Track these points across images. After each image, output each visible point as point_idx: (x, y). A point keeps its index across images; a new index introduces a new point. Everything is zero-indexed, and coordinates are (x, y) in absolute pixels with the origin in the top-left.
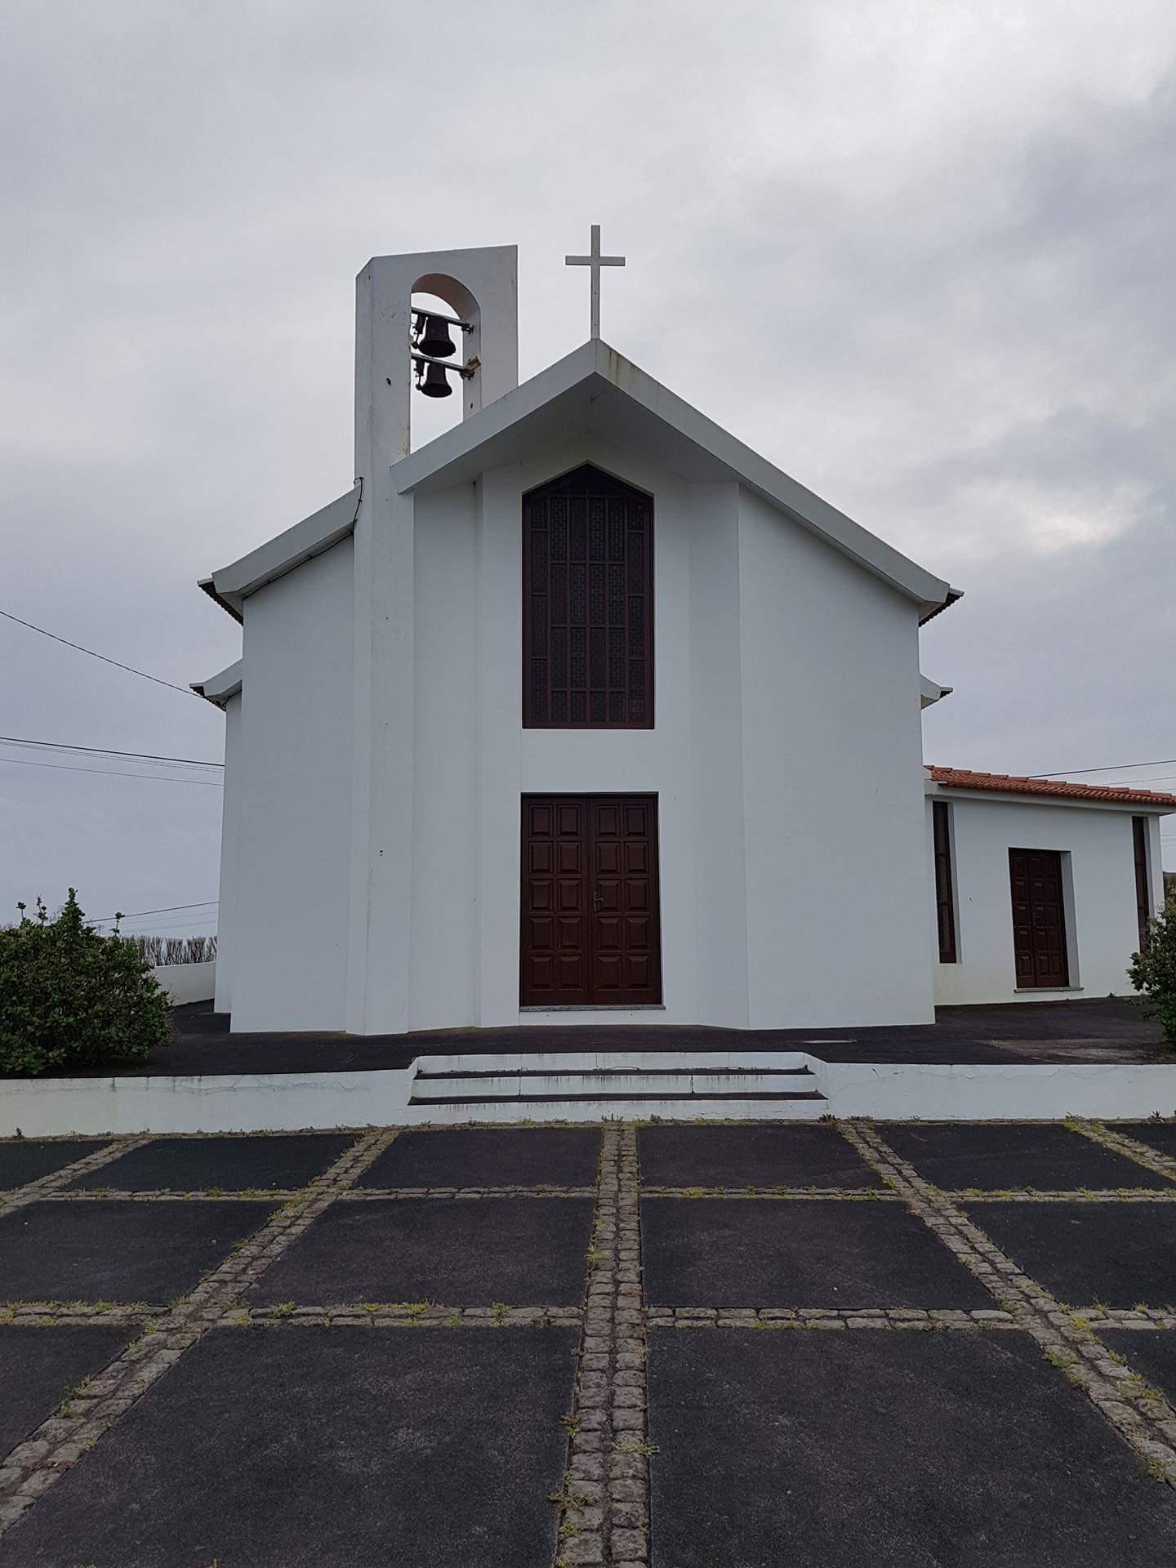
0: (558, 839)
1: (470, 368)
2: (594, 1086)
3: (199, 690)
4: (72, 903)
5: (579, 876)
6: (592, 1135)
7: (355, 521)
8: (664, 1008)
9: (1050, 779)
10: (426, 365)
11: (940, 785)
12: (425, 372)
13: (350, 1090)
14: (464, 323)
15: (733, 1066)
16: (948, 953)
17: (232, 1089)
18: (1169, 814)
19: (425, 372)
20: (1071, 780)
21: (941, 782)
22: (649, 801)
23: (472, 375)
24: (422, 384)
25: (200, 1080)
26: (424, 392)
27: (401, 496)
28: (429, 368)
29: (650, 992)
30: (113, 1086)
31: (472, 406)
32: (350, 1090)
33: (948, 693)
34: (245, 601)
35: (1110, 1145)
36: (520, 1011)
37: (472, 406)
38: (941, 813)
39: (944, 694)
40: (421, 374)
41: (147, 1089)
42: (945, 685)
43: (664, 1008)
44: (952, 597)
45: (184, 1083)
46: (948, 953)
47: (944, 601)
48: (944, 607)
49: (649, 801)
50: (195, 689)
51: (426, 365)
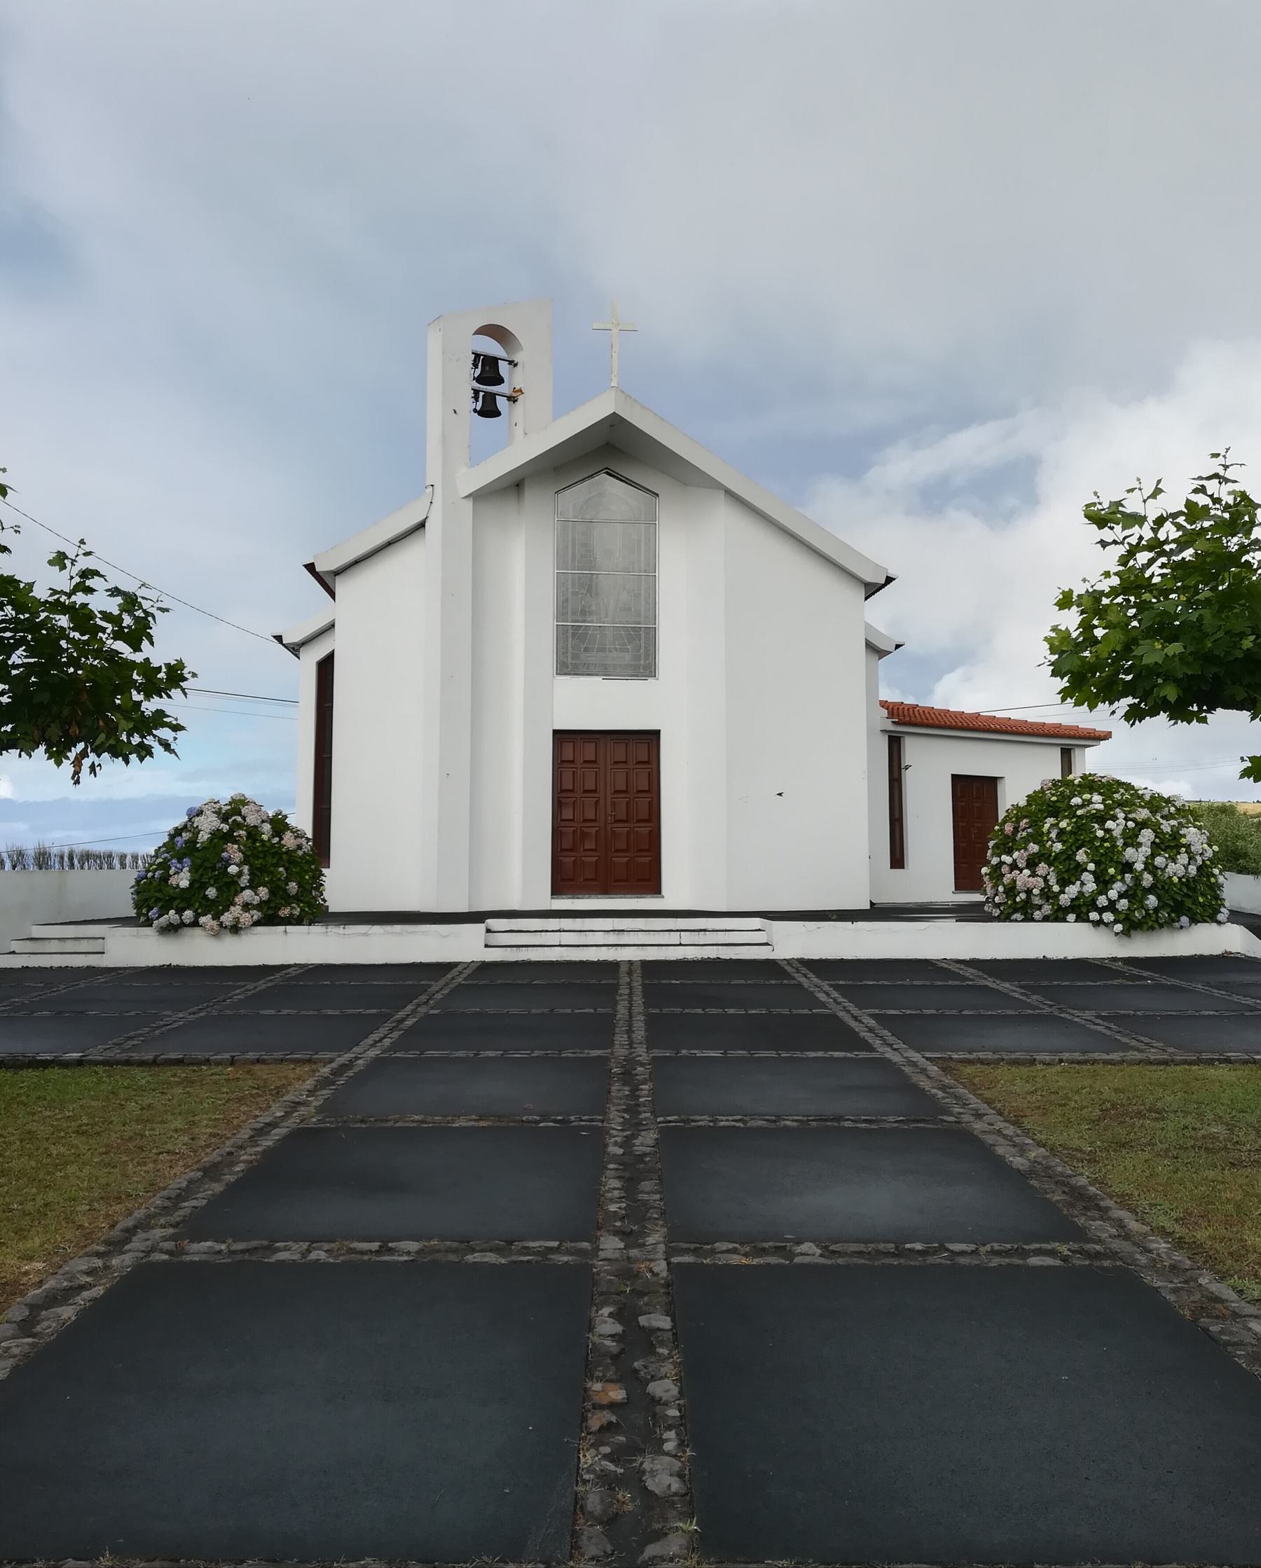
0: (635, 767)
1: (514, 395)
2: (612, 939)
3: (279, 638)
4: (1251, 721)
5: (597, 795)
6: (613, 966)
7: (427, 518)
8: (663, 897)
9: (998, 715)
10: (481, 394)
11: (893, 722)
12: (480, 399)
13: (446, 936)
14: (510, 359)
15: (709, 928)
16: (898, 860)
17: (366, 934)
18: (1093, 746)
19: (480, 399)
20: (1015, 715)
21: (894, 720)
22: (652, 737)
23: (516, 401)
24: (478, 409)
25: (344, 928)
26: (479, 415)
27: (464, 500)
28: (483, 396)
29: (652, 884)
30: (285, 931)
31: (516, 425)
32: (446, 936)
33: (902, 645)
34: (337, 577)
35: (955, 970)
36: (552, 898)
37: (516, 425)
38: (895, 744)
39: (898, 646)
40: (477, 400)
41: (309, 933)
42: (899, 642)
43: (663, 897)
44: (889, 580)
45: (333, 930)
46: (898, 860)
47: (883, 583)
48: (883, 586)
49: (652, 737)
50: (275, 637)
51: (481, 394)
